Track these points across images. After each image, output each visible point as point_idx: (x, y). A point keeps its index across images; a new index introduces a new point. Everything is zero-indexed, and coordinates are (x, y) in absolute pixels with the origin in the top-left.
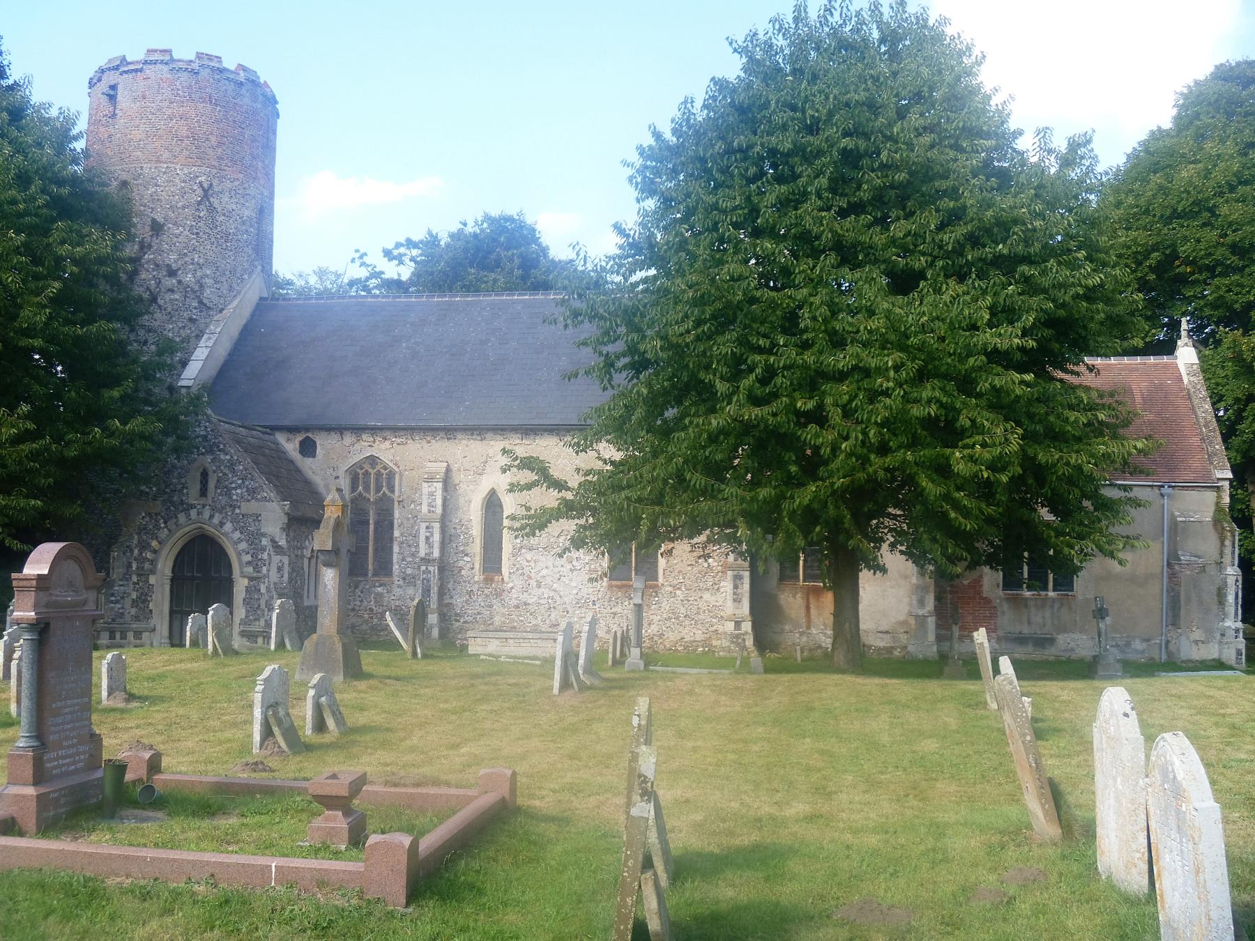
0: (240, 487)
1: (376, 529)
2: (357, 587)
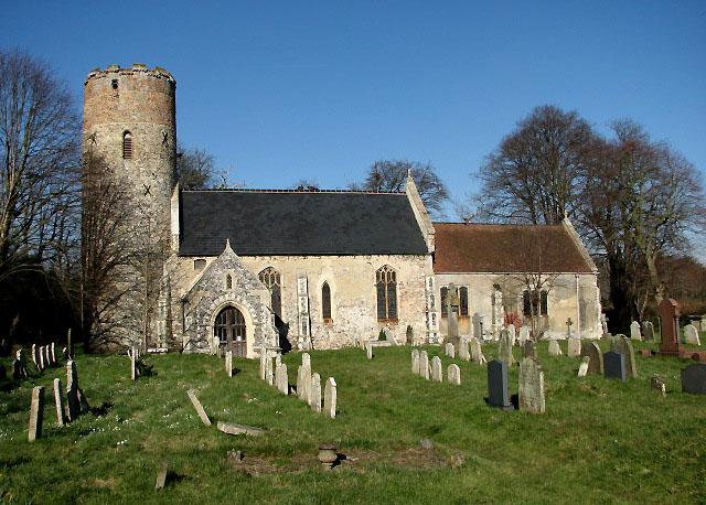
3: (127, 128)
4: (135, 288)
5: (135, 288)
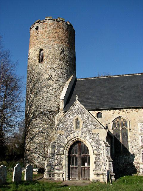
0: (91, 125)
1: (122, 139)
2: (118, 157)
3: (41, 47)
4: (42, 132)
5: (42, 132)
